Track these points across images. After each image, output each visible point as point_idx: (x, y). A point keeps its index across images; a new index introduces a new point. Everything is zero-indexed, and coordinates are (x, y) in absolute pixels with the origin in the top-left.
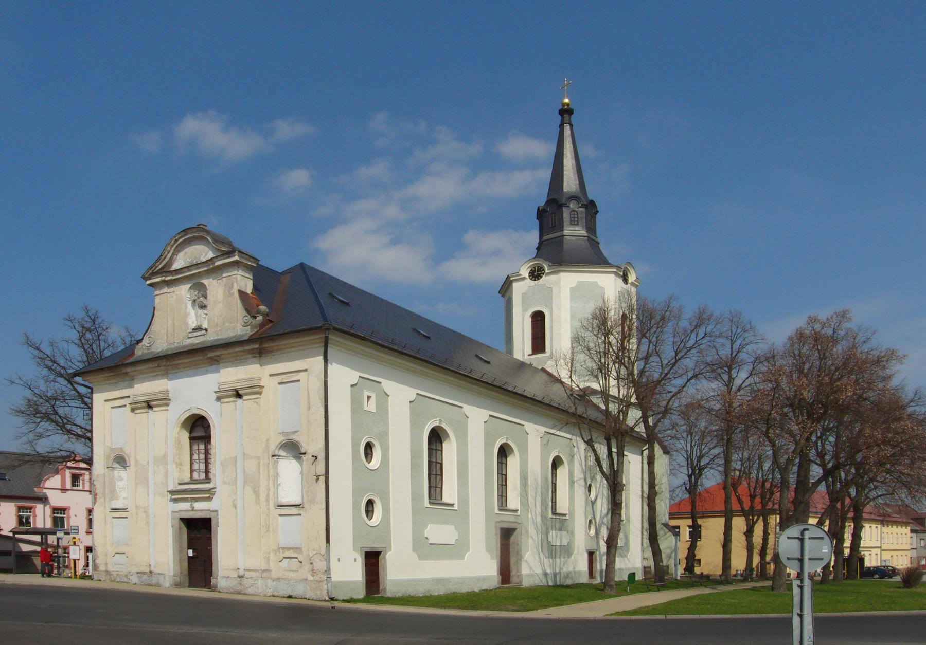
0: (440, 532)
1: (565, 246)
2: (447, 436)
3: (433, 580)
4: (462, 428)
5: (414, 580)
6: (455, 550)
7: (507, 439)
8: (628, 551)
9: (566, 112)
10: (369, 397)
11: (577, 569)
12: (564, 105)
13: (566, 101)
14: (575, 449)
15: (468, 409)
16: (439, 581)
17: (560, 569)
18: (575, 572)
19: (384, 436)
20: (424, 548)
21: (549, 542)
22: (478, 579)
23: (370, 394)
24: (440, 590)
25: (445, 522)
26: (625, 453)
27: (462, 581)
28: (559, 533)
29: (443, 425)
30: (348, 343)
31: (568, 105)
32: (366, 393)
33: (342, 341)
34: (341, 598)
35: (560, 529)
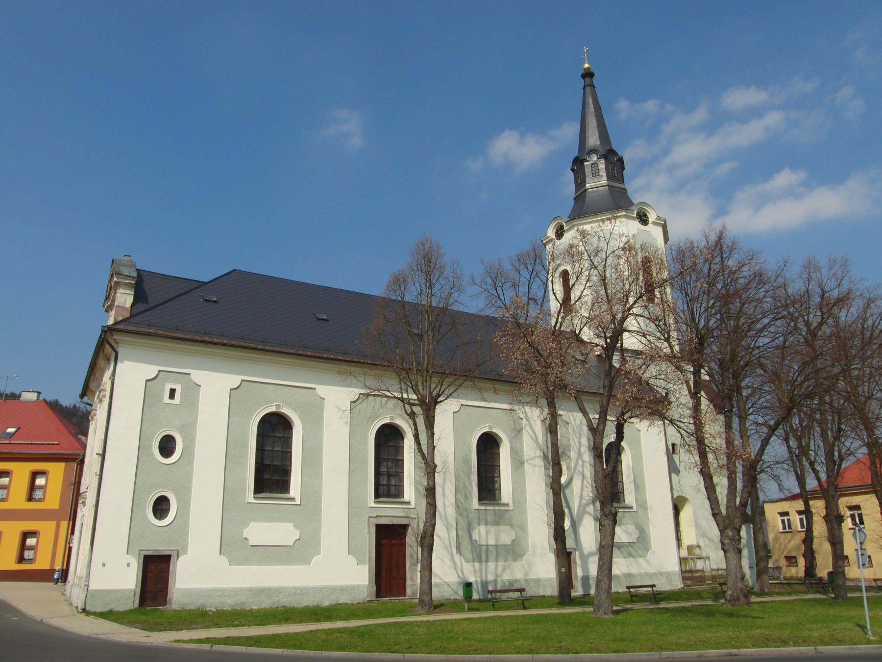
0: (270, 528)
1: (587, 200)
2: (501, 439)
3: (250, 590)
4: (315, 413)
5: (218, 590)
6: (301, 552)
7: (391, 418)
8: (647, 548)
9: (588, 75)
10: (172, 393)
11: (532, 576)
12: (585, 69)
13: (586, 66)
14: (524, 421)
15: (322, 390)
16: (260, 591)
17: (497, 576)
18: (526, 580)
19: (189, 429)
20: (233, 547)
21: (473, 542)
22: (343, 589)
23: (173, 387)
24: (265, 603)
25: (280, 519)
26: (560, 412)
27: (304, 591)
28: (492, 529)
29: (495, 430)
30: (144, 341)
31: (588, 68)
32: (168, 387)
33: (130, 339)
34: (99, 610)
35: (496, 523)
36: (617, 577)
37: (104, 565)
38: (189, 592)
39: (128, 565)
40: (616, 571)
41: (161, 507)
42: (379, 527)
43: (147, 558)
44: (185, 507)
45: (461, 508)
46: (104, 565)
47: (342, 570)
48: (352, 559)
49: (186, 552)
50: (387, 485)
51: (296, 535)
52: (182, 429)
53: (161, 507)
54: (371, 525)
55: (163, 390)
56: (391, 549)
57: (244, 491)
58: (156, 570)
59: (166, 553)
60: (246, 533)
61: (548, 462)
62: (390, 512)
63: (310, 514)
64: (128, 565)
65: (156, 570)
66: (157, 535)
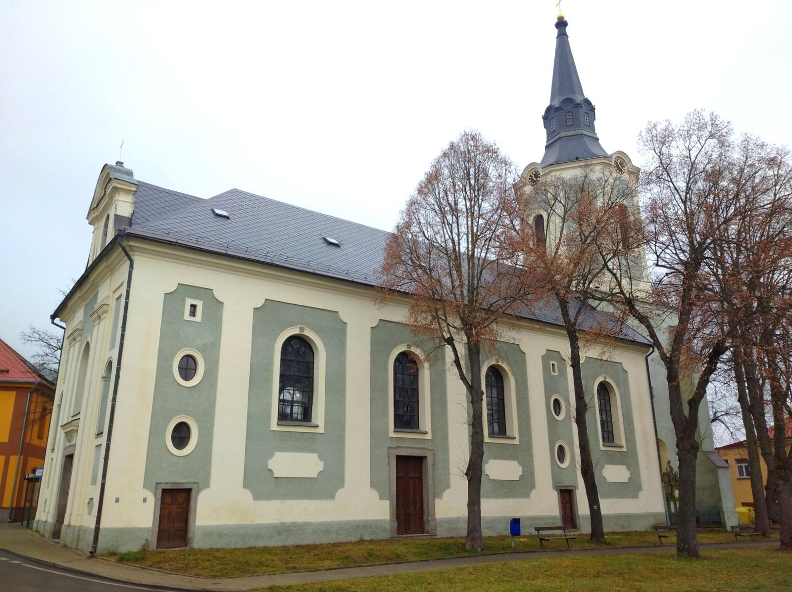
19: (212, 350)
32: (189, 302)
36: (604, 517)
37: (117, 500)
38: (209, 532)
39: (145, 500)
40: (604, 511)
41: (181, 435)
42: (399, 458)
43: (165, 491)
44: (155, 432)
45: (255, 420)
46: (117, 500)
47: (363, 503)
48: (375, 494)
49: (207, 486)
50: (407, 418)
51: (319, 466)
52: (203, 350)
53: (181, 435)
54: (391, 457)
55: (184, 306)
56: (410, 479)
57: (269, 417)
58: (176, 503)
59: (186, 487)
60: (272, 464)
61: (243, 576)
62: (409, 443)
63: (333, 447)
64: (145, 500)
65: (176, 503)
66: (178, 466)
